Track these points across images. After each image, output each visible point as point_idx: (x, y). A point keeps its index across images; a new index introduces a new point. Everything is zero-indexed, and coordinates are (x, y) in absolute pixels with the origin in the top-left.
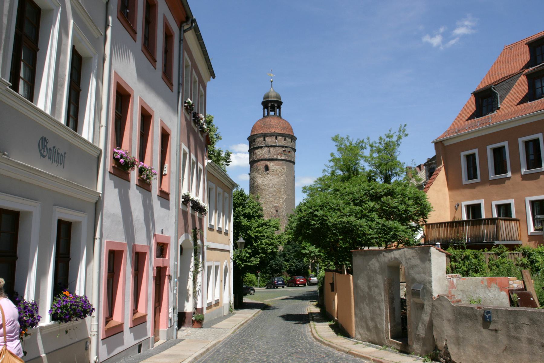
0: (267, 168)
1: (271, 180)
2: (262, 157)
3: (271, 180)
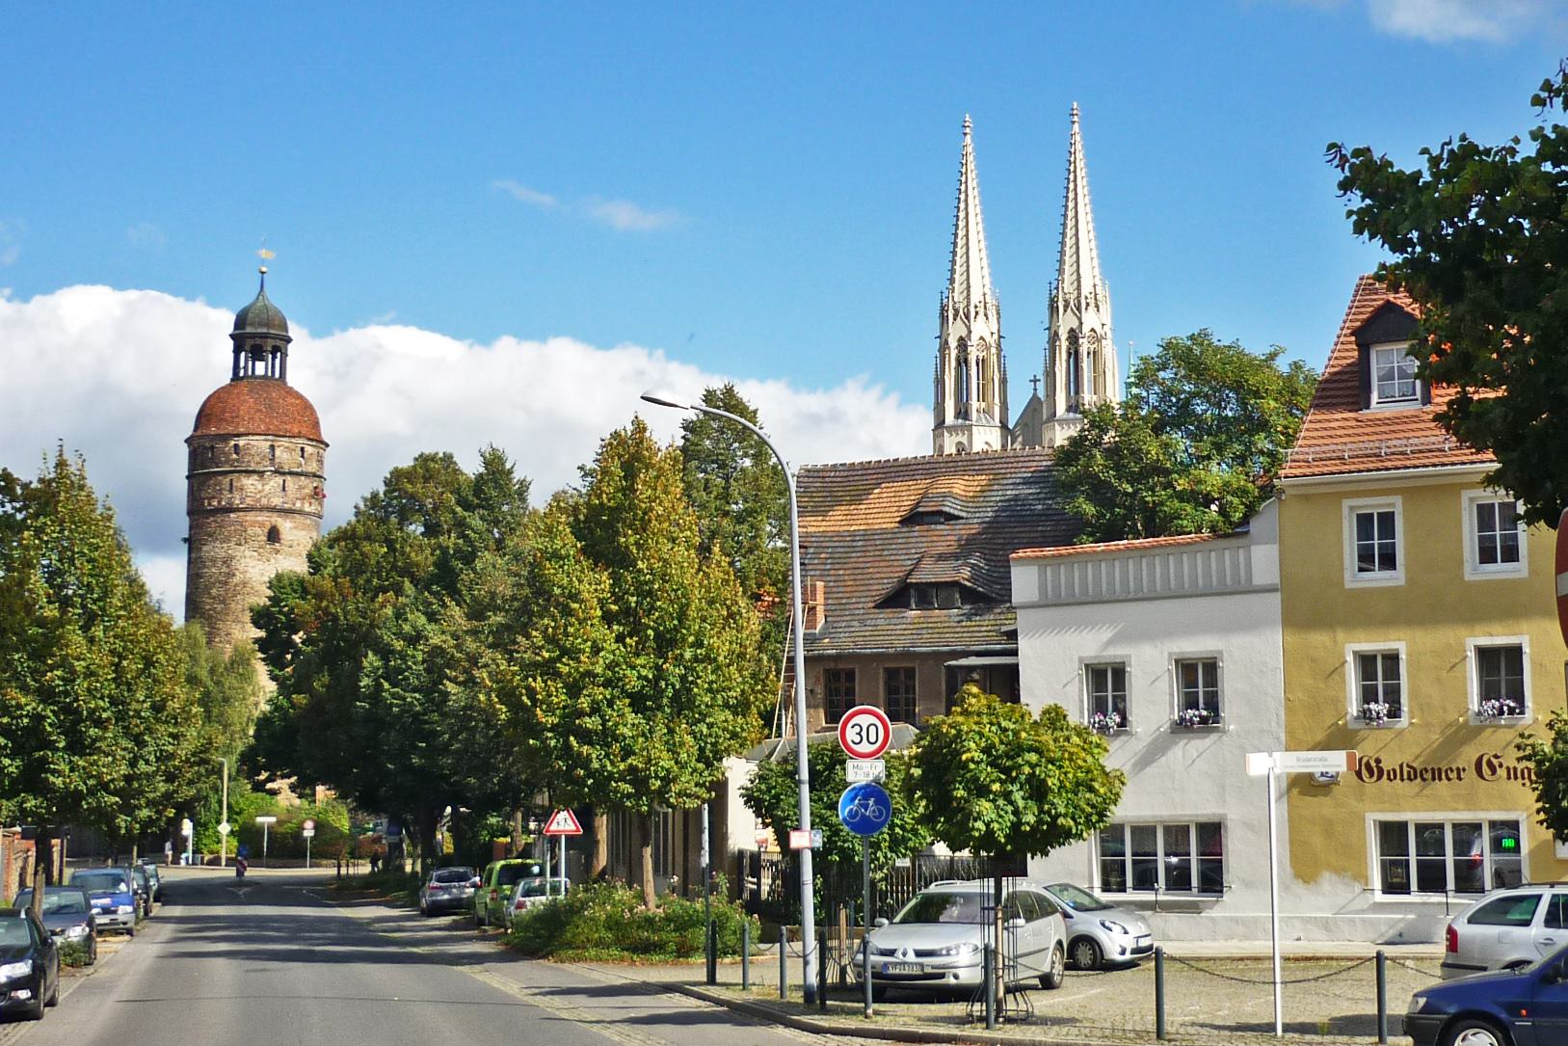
2: (264, 501)
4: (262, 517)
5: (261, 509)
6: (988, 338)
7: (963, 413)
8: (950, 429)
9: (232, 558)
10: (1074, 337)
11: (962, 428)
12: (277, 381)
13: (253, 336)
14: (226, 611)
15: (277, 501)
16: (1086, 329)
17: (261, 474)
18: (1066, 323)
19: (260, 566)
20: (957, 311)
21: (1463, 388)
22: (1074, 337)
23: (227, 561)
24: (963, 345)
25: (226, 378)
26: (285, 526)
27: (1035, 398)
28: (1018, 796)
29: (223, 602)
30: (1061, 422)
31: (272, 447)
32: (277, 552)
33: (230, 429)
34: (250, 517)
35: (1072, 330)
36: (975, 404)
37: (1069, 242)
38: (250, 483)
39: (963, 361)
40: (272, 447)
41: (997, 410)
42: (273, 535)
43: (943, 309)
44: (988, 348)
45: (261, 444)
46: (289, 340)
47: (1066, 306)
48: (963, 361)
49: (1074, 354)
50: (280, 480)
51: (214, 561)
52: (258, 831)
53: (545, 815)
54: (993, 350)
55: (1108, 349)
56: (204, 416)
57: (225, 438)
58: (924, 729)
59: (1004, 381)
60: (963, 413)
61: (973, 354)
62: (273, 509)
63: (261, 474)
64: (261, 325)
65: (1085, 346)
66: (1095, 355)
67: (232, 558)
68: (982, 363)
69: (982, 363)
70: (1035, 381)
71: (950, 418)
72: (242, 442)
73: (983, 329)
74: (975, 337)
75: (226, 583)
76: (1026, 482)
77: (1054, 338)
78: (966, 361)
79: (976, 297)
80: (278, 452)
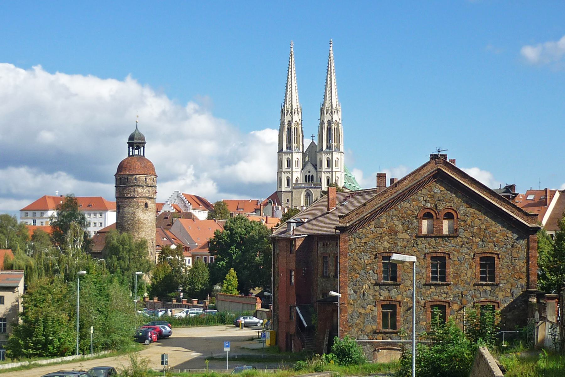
4: (143, 200)
5: (143, 197)
6: (298, 121)
7: (289, 147)
8: (285, 153)
10: (329, 123)
11: (289, 153)
12: (142, 157)
13: (137, 143)
14: (133, 228)
15: (147, 195)
16: (334, 120)
17: (143, 186)
18: (327, 118)
20: (288, 111)
22: (329, 123)
23: (133, 213)
24: (290, 123)
25: (127, 157)
26: (149, 202)
27: (313, 143)
28: (60, 296)
29: (132, 226)
30: (325, 152)
32: (147, 210)
33: (133, 173)
34: (140, 200)
35: (329, 120)
36: (294, 145)
37: (328, 89)
38: (140, 189)
39: (290, 129)
41: (301, 147)
42: (146, 205)
43: (282, 111)
44: (298, 125)
45: (142, 177)
46: (145, 143)
47: (327, 112)
49: (329, 129)
50: (148, 188)
51: (129, 213)
52: (432, 277)
54: (300, 126)
55: (341, 128)
56: (121, 167)
57: (133, 175)
59: (303, 136)
60: (289, 147)
61: (293, 126)
63: (143, 186)
64: (139, 139)
65: (333, 126)
66: (336, 129)
68: (296, 130)
69: (296, 130)
71: (285, 149)
72: (137, 177)
73: (296, 118)
74: (294, 121)
76: (336, 180)
77: (322, 123)
79: (294, 107)
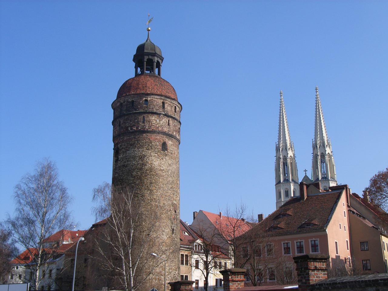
0: (164, 146)
1: (170, 165)
2: (160, 129)
3: (170, 165)
9: (145, 156)
15: (166, 129)
19: (9, 241)
21: (367, 195)
23: (142, 157)
25: (133, 75)
31: (163, 103)
32: (166, 155)
38: (153, 118)
39: (285, 164)
40: (163, 103)
45: (158, 101)
48: (285, 164)
53: (154, 284)
58: (31, 271)
62: (164, 133)
67: (145, 156)
70: (305, 171)
75: (141, 169)
78: (286, 163)
80: (166, 106)
